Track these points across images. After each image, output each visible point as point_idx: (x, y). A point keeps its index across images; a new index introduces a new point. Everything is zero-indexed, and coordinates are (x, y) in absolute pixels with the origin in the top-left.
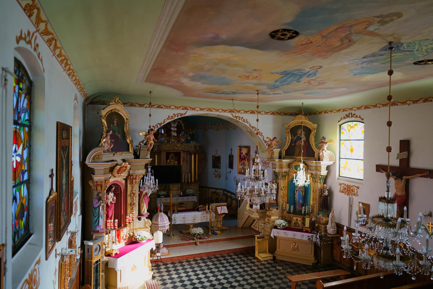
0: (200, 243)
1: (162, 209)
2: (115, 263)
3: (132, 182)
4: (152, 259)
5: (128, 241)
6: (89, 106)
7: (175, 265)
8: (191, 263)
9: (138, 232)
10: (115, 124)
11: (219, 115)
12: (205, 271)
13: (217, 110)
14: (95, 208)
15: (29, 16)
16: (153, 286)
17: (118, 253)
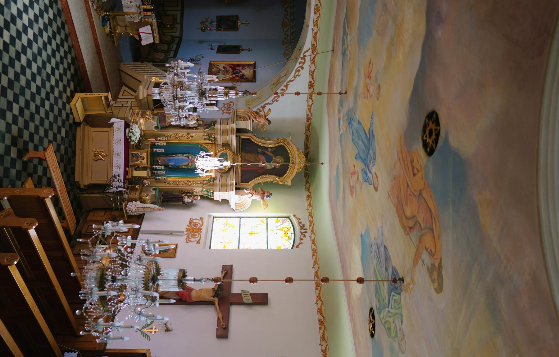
11: (308, 26)
13: (316, 24)
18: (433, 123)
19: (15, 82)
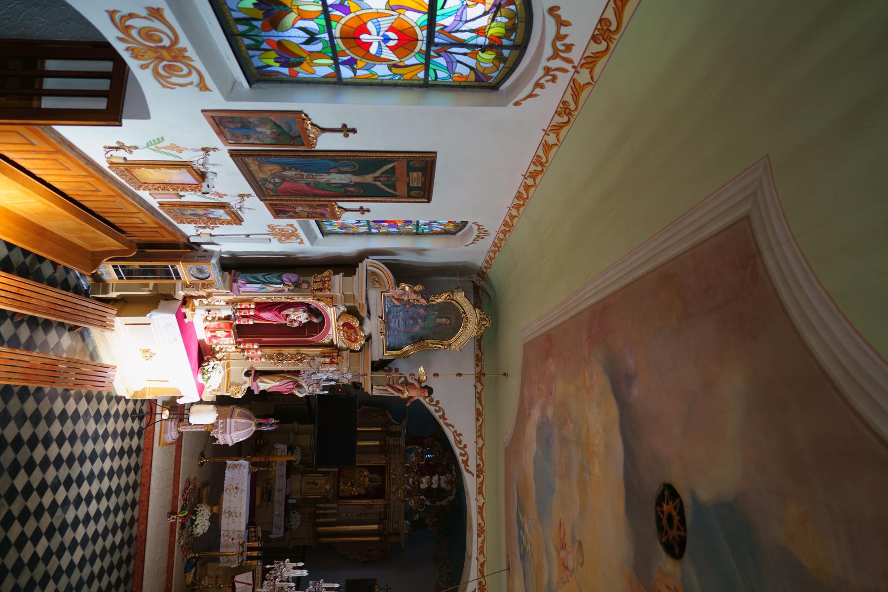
0: (173, 525)
1: (264, 428)
2: (166, 310)
3: (325, 357)
4: (160, 403)
5: (206, 346)
6: (471, 284)
7: (134, 455)
8: (131, 491)
9: (220, 368)
10: (439, 321)
11: (470, 558)
12: (102, 519)
13: (481, 551)
14: (280, 277)
15: (594, 38)
16: (103, 374)
17: (186, 321)
18: (668, 504)
19: (32, 517)
